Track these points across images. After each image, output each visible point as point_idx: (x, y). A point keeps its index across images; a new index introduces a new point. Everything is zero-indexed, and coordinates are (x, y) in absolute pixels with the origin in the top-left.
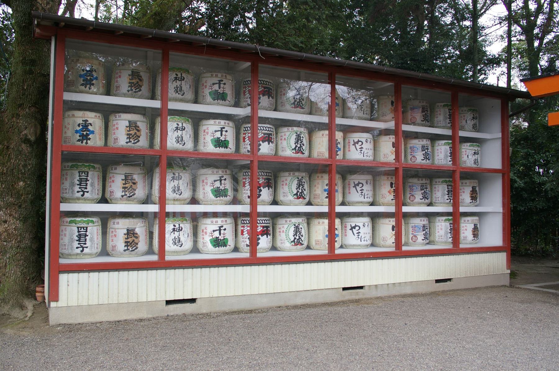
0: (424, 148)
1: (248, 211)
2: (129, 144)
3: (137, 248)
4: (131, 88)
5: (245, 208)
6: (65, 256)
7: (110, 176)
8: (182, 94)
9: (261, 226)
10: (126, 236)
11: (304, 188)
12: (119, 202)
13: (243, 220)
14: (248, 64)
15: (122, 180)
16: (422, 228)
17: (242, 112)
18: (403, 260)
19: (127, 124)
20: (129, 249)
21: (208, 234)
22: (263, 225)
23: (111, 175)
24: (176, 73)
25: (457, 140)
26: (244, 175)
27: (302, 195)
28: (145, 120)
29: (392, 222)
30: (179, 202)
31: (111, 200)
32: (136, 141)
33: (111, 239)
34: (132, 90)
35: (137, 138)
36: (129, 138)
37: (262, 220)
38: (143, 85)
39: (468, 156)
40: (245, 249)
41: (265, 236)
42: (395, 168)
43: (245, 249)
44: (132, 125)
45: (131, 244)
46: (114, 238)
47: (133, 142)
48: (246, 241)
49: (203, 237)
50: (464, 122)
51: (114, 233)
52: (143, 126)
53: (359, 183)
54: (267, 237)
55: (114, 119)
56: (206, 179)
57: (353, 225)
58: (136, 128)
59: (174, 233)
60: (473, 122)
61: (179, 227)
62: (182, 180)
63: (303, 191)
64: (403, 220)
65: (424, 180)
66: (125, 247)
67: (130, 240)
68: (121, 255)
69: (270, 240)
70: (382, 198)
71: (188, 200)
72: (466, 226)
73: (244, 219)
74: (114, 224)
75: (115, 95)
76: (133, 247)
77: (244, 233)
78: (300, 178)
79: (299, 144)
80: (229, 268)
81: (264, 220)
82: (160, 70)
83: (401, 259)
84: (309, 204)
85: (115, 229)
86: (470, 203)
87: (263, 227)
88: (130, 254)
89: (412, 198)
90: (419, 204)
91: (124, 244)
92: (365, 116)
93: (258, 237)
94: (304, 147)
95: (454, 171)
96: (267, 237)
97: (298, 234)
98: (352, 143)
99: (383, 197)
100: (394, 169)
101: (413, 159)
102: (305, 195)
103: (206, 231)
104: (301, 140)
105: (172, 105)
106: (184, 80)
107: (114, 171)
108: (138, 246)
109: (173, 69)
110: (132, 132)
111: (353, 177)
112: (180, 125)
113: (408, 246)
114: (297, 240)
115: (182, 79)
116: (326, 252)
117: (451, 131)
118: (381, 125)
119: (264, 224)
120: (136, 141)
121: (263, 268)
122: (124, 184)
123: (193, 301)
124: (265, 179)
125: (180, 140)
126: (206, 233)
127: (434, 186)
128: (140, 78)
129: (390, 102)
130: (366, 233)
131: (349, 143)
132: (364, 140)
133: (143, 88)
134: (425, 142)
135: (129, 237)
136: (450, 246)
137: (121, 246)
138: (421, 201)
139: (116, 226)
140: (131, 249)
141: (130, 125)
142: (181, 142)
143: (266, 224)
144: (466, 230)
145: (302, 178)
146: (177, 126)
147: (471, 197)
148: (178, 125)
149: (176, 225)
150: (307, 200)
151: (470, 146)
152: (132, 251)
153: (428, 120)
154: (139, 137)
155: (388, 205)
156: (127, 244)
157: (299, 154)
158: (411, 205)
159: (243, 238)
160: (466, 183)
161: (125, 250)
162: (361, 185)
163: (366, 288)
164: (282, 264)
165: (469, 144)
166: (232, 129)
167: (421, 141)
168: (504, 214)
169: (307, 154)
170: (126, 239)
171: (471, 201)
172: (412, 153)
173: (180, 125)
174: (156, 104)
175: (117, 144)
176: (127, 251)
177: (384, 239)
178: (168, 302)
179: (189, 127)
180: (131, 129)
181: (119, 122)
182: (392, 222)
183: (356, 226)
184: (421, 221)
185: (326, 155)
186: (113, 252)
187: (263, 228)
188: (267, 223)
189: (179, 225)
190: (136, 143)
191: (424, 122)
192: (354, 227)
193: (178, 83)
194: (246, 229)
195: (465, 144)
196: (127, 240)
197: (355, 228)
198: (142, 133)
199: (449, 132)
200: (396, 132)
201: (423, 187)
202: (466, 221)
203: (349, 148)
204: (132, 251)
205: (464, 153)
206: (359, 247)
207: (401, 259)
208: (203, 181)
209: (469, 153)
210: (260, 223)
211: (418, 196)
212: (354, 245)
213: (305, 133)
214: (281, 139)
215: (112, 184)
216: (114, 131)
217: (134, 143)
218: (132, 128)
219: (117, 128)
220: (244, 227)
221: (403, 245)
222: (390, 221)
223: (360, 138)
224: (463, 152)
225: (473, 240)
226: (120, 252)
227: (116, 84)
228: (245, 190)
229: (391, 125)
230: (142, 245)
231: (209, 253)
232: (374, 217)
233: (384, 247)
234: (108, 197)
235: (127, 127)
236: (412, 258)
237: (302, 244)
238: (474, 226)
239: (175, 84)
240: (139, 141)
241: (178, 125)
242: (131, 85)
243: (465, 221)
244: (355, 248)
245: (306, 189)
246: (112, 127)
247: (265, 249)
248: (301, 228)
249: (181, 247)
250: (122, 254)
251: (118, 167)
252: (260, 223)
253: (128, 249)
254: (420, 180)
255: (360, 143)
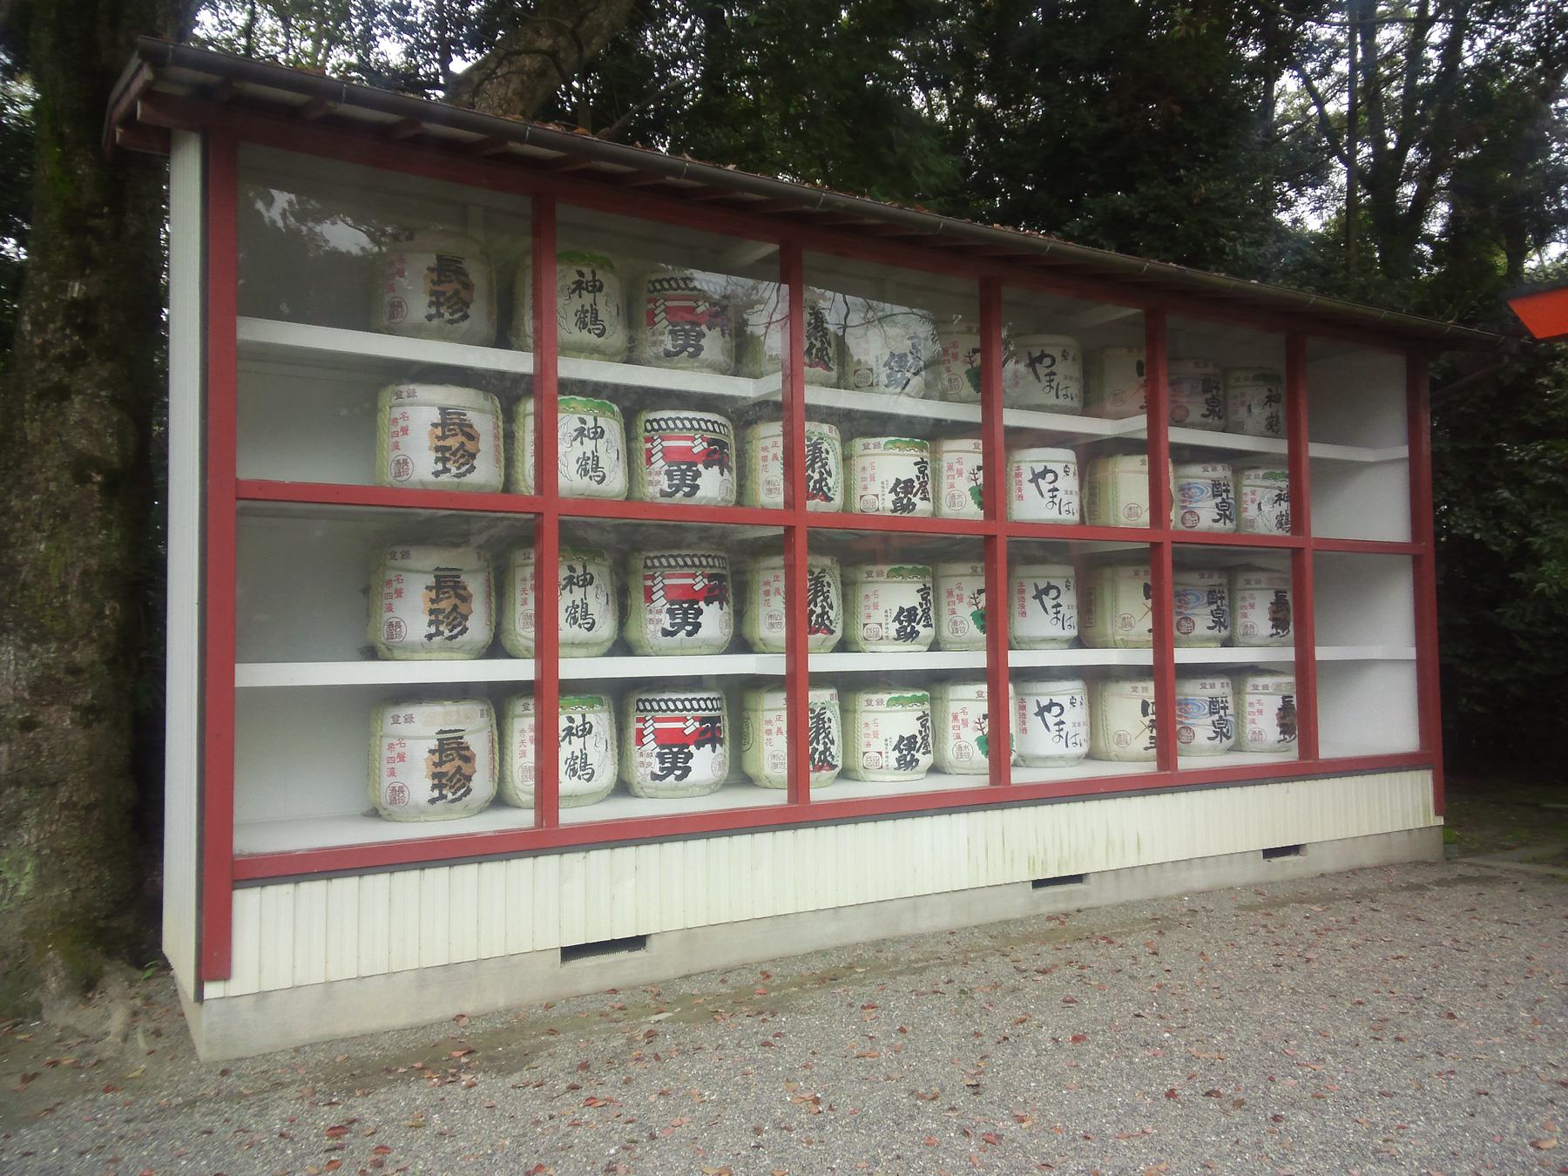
0: (1217, 488)
1: (531, 676)
2: (444, 478)
3: (469, 791)
4: (438, 311)
5: (522, 670)
6: (1025, 761)
7: (387, 578)
8: (597, 332)
9: (695, 718)
10: (436, 758)
11: (829, 601)
12: (416, 656)
13: (640, 700)
14: (771, 248)
15: (427, 588)
16: (1207, 707)
17: (519, 362)
18: (1183, 798)
19: (437, 418)
20: (445, 797)
21: (971, 724)
22: (700, 713)
23: (391, 575)
24: (579, 269)
25: (1000, 437)
26: (646, 566)
27: (823, 623)
28: (488, 405)
29: (1148, 690)
30: (583, 651)
31: (388, 649)
32: (464, 469)
33: (386, 767)
34: (440, 315)
35: (468, 457)
36: (444, 460)
37: (698, 701)
38: (472, 301)
39: (1259, 504)
40: (648, 787)
41: (708, 746)
42: (1152, 543)
43: (648, 787)
44: (452, 424)
45: (450, 780)
46: (398, 766)
47: (454, 471)
48: (650, 764)
49: (390, 766)
50: (1243, 412)
51: (398, 749)
52: (484, 422)
53: (1050, 587)
54: (714, 751)
55: (394, 402)
56: (959, 587)
57: (1045, 702)
58: (462, 430)
59: (570, 743)
60: (1267, 412)
61: (584, 724)
62: (594, 585)
63: (827, 609)
64: (1011, 687)
65: (1216, 576)
66: (433, 790)
67: (448, 768)
68: (418, 814)
69: (720, 759)
70: (1124, 626)
71: (608, 645)
72: (1259, 702)
73: (644, 697)
74: (396, 722)
75: (391, 331)
76: (459, 789)
77: (645, 740)
78: (817, 571)
79: (817, 470)
80: (736, 839)
81: (705, 700)
82: (529, 261)
83: (1055, 806)
84: (935, 646)
85: (401, 738)
86: (1272, 635)
87: (703, 720)
88: (449, 811)
89: (1185, 625)
90: (1204, 641)
91: (429, 783)
92: (1068, 403)
93: (686, 750)
94: (830, 481)
95: (990, 540)
96: (714, 751)
97: (821, 737)
98: (1027, 475)
99: (1127, 623)
100: (1148, 546)
101: (1189, 518)
102: (831, 622)
103: (965, 717)
104: (821, 460)
105: (570, 368)
106: (600, 289)
107: (400, 563)
108: (472, 784)
109: (570, 257)
110: (453, 442)
111: (1037, 570)
112: (590, 423)
113: (1241, 751)
114: (821, 753)
115: (597, 288)
116: (983, 781)
117: (979, 409)
118: (1103, 428)
119: (704, 710)
120: (464, 469)
121: (828, 833)
122: (432, 601)
123: (637, 942)
124: (711, 577)
125: (590, 466)
126: (965, 723)
127: (1239, 595)
128: (462, 278)
129: (1135, 366)
130: (1079, 724)
131: (1019, 475)
132: (1059, 469)
133: (472, 310)
134: (1221, 472)
135: (444, 759)
136: (1150, 767)
137: (420, 787)
138: (1210, 632)
139: (403, 729)
140: (450, 796)
141: (443, 418)
142: (593, 474)
143: (710, 710)
144: (1260, 712)
145: (823, 571)
146: (579, 425)
147: (1273, 619)
148: (583, 421)
149: (573, 716)
150: (838, 634)
151: (1265, 477)
152: (453, 801)
153: (1218, 416)
154: (473, 456)
155: (1137, 645)
156: (440, 780)
157: (817, 500)
158: (1023, 646)
159: (641, 755)
160: (1258, 582)
161: (433, 801)
162: (1053, 593)
163: (1092, 879)
164: (836, 825)
165: (1261, 473)
166: (490, 417)
167: (1210, 469)
168: (1421, 662)
169: (838, 500)
170: (436, 765)
171: (1274, 631)
172: (1187, 504)
173: (590, 423)
174: (519, 362)
175: (405, 477)
176: (439, 803)
177: (1121, 739)
178: (569, 953)
179: (613, 427)
180: (447, 433)
181: (408, 409)
182: (1148, 690)
183: (1052, 704)
184: (1204, 687)
185: (1144, 519)
186: (393, 808)
187: (701, 725)
188: (713, 709)
189: (584, 716)
190: (464, 475)
191: (1210, 420)
192: (1048, 708)
193: (587, 298)
194: (652, 729)
195: (1252, 473)
196: (439, 770)
197: (1049, 711)
198: (481, 445)
199: (973, 414)
200: (1149, 447)
201: (1212, 596)
202: (1260, 688)
203: (1020, 490)
204: (453, 801)
205: (1250, 497)
206: (1061, 763)
207: (1040, 808)
208: (950, 593)
209: (1263, 497)
210: (693, 709)
211: (1202, 621)
212: (1047, 758)
213: (832, 439)
214: (765, 459)
215: (396, 602)
216: (394, 440)
217: (457, 476)
218: (450, 430)
219: (405, 430)
220: (644, 720)
221: (1016, 765)
222: (1135, 689)
223: (1051, 461)
224: (1246, 494)
225: (1279, 742)
226: (417, 806)
227: (388, 297)
228: (651, 612)
229: (1136, 425)
230: (482, 786)
231: (970, 772)
232: (1097, 679)
233: (1119, 759)
234: (383, 639)
235: (435, 425)
236: (1103, 802)
237: (833, 767)
238: (1284, 701)
239: (577, 303)
240: (472, 469)
241: (583, 421)
242: (437, 300)
243: (1255, 687)
244: (1049, 764)
245: (835, 605)
246: (389, 429)
247: (708, 786)
248: (830, 720)
249: (589, 780)
250: (422, 812)
251: (414, 553)
252: (693, 709)
253: (442, 797)
254: (1206, 576)
255: (1050, 477)
